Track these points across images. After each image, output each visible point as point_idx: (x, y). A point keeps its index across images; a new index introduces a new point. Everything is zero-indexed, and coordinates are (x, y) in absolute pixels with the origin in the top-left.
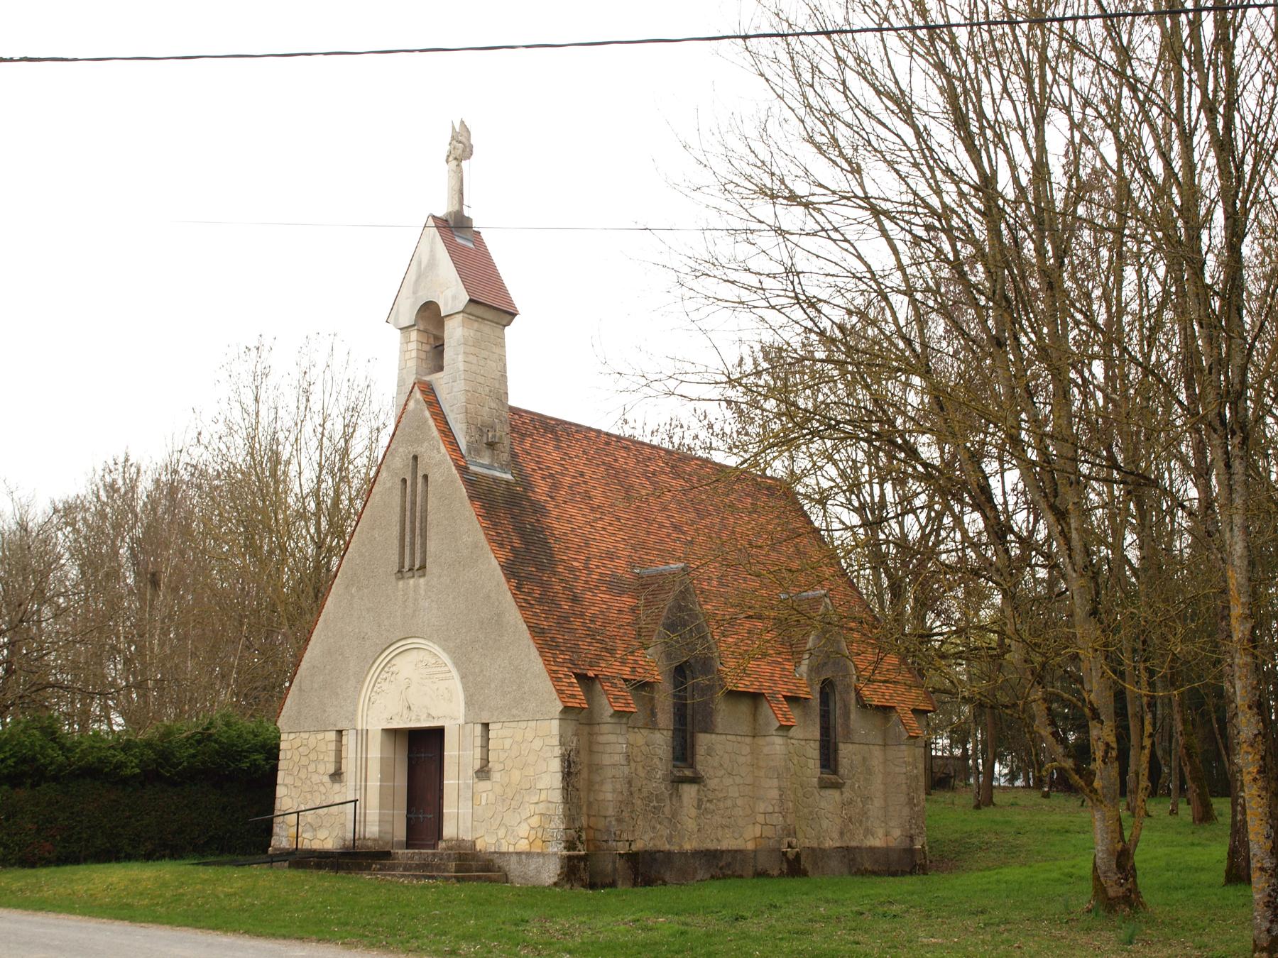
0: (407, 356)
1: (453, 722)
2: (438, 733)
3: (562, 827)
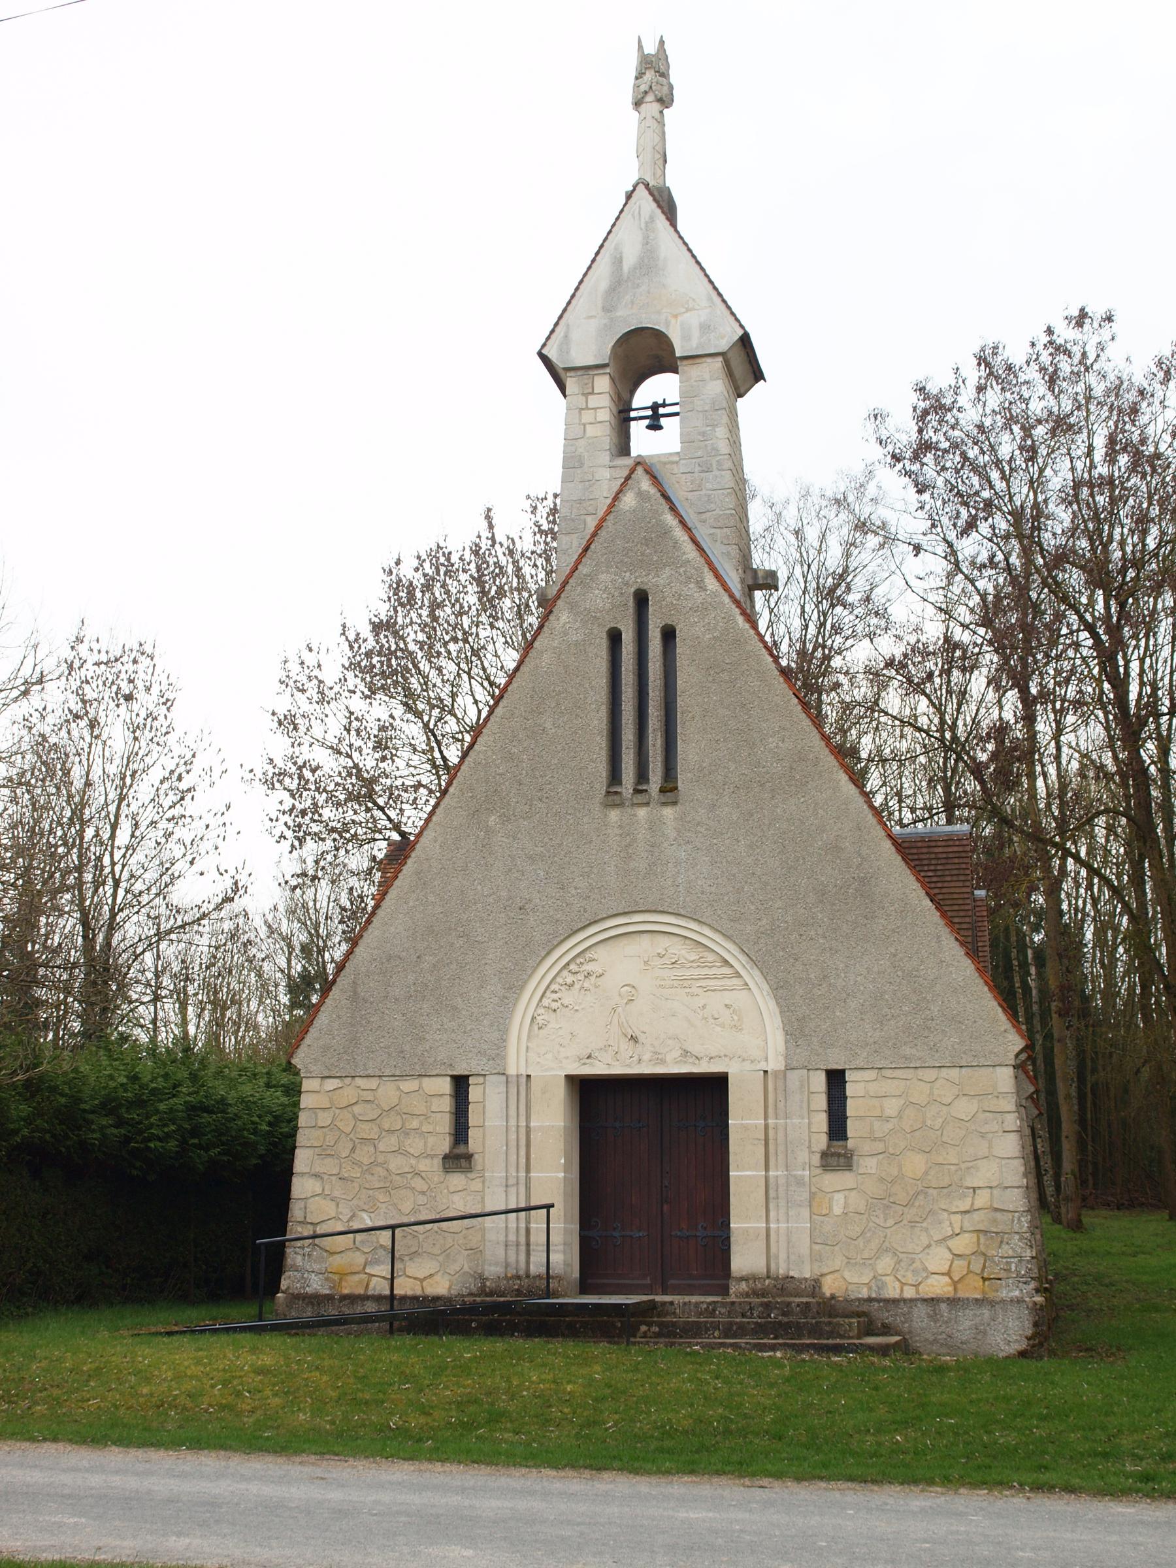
0: (587, 417)
1: (748, 1066)
2: (714, 1088)
3: (1028, 1253)
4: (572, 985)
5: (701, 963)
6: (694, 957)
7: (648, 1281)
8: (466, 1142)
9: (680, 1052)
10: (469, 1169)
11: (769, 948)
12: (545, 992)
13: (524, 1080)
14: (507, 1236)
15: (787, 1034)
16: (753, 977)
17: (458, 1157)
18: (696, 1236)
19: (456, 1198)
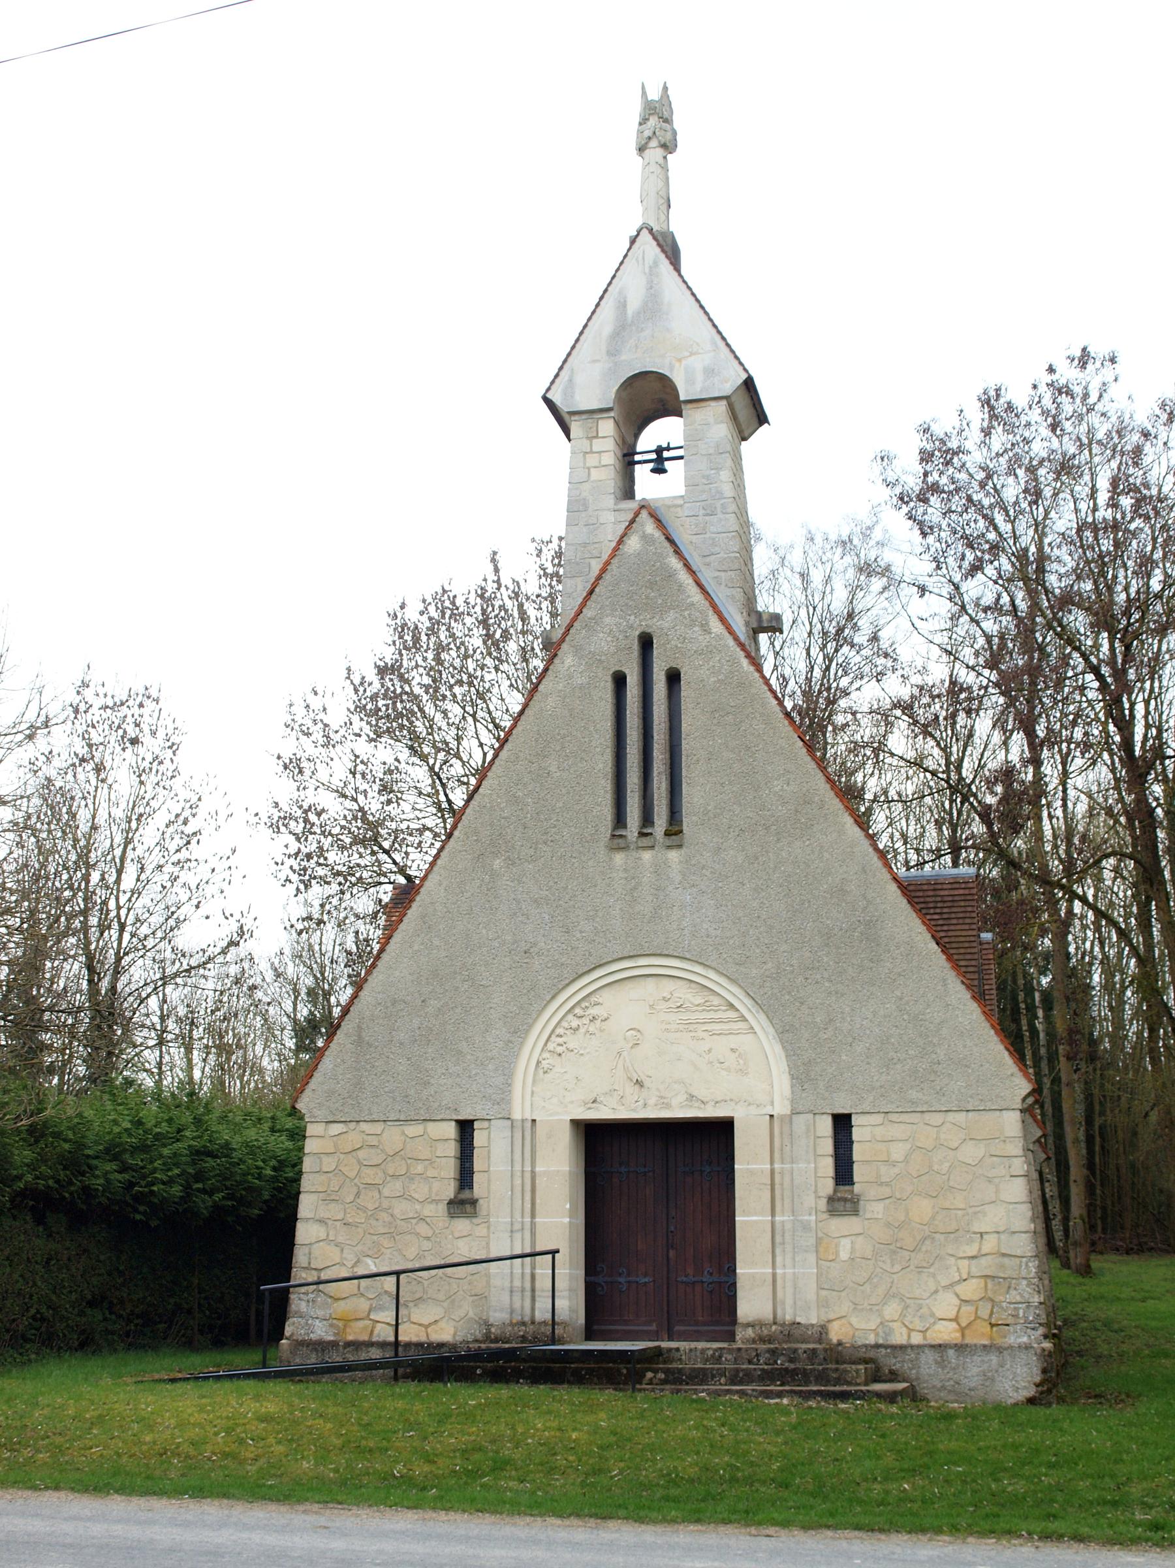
1: (753, 1110)
2: (720, 1132)
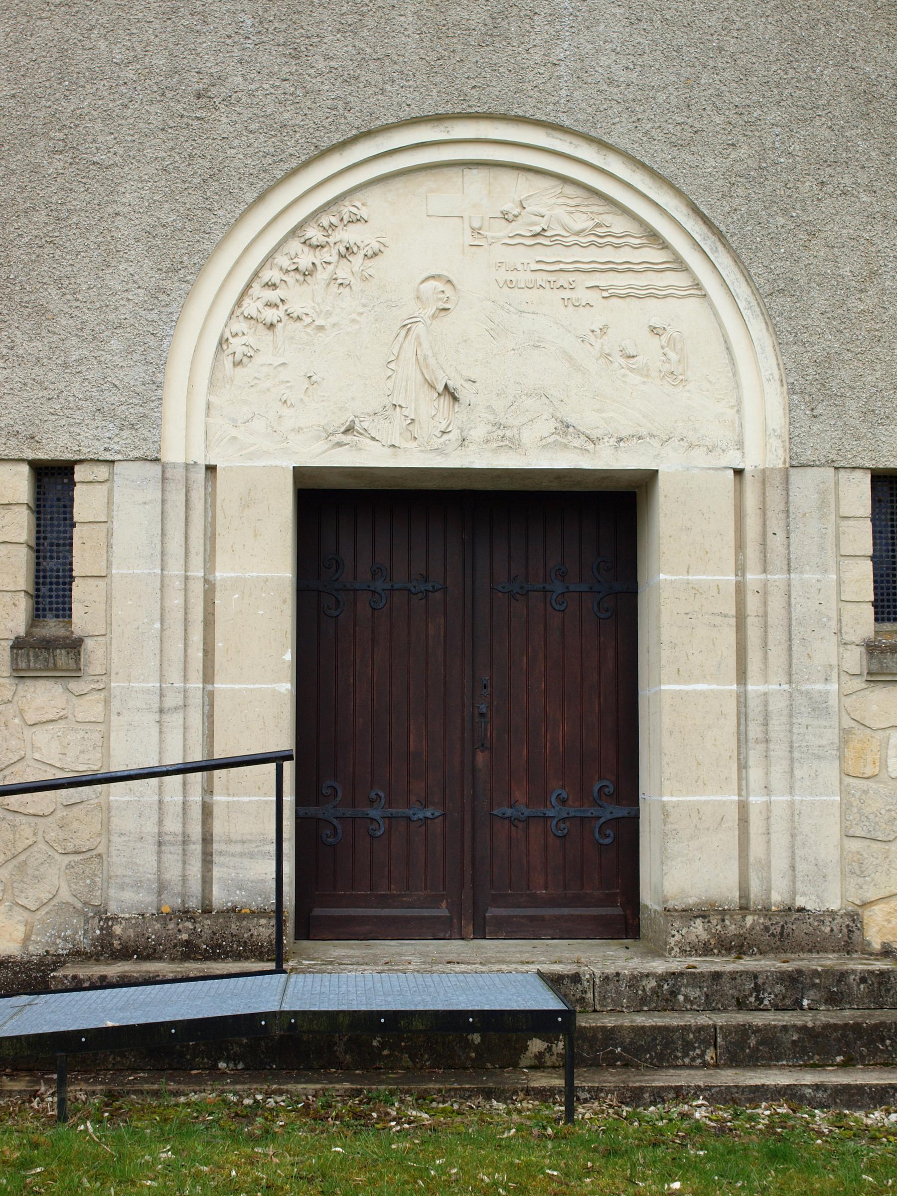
1: (700, 458)
4: (308, 274)
5: (599, 238)
6: (581, 222)
7: (443, 911)
8: (64, 611)
9: (552, 424)
10: (75, 672)
11: (757, 206)
12: (249, 286)
13: (200, 475)
14: (160, 822)
15: (792, 391)
16: (714, 271)
17: (48, 645)
18: (546, 818)
19: (41, 736)
